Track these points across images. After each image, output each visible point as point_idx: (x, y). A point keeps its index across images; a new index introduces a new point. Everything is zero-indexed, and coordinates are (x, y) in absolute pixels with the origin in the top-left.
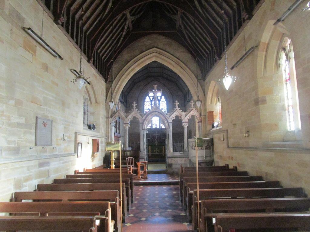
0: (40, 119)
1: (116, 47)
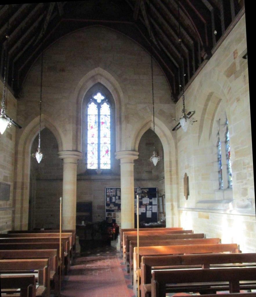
0: (173, 226)
1: (35, 41)
